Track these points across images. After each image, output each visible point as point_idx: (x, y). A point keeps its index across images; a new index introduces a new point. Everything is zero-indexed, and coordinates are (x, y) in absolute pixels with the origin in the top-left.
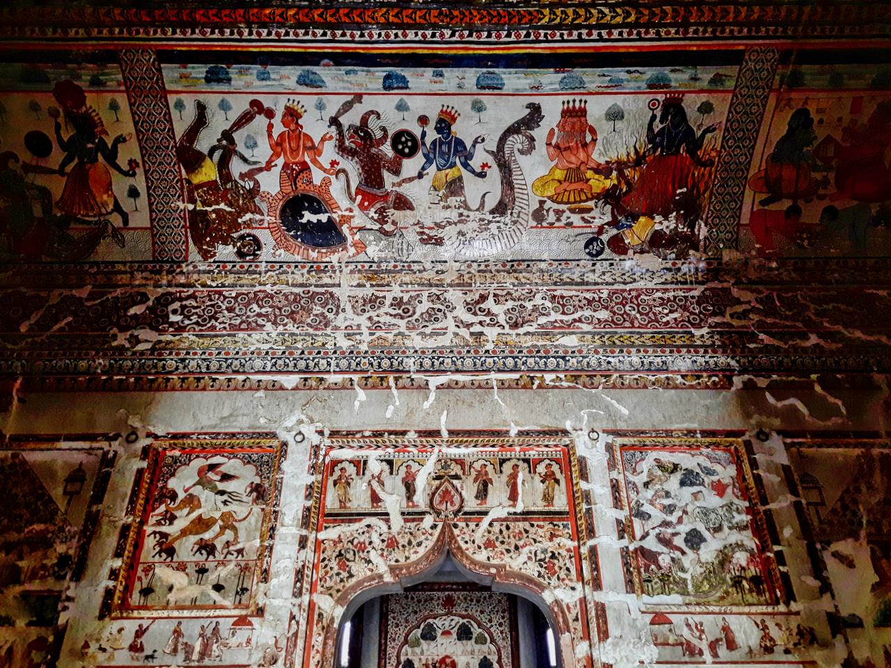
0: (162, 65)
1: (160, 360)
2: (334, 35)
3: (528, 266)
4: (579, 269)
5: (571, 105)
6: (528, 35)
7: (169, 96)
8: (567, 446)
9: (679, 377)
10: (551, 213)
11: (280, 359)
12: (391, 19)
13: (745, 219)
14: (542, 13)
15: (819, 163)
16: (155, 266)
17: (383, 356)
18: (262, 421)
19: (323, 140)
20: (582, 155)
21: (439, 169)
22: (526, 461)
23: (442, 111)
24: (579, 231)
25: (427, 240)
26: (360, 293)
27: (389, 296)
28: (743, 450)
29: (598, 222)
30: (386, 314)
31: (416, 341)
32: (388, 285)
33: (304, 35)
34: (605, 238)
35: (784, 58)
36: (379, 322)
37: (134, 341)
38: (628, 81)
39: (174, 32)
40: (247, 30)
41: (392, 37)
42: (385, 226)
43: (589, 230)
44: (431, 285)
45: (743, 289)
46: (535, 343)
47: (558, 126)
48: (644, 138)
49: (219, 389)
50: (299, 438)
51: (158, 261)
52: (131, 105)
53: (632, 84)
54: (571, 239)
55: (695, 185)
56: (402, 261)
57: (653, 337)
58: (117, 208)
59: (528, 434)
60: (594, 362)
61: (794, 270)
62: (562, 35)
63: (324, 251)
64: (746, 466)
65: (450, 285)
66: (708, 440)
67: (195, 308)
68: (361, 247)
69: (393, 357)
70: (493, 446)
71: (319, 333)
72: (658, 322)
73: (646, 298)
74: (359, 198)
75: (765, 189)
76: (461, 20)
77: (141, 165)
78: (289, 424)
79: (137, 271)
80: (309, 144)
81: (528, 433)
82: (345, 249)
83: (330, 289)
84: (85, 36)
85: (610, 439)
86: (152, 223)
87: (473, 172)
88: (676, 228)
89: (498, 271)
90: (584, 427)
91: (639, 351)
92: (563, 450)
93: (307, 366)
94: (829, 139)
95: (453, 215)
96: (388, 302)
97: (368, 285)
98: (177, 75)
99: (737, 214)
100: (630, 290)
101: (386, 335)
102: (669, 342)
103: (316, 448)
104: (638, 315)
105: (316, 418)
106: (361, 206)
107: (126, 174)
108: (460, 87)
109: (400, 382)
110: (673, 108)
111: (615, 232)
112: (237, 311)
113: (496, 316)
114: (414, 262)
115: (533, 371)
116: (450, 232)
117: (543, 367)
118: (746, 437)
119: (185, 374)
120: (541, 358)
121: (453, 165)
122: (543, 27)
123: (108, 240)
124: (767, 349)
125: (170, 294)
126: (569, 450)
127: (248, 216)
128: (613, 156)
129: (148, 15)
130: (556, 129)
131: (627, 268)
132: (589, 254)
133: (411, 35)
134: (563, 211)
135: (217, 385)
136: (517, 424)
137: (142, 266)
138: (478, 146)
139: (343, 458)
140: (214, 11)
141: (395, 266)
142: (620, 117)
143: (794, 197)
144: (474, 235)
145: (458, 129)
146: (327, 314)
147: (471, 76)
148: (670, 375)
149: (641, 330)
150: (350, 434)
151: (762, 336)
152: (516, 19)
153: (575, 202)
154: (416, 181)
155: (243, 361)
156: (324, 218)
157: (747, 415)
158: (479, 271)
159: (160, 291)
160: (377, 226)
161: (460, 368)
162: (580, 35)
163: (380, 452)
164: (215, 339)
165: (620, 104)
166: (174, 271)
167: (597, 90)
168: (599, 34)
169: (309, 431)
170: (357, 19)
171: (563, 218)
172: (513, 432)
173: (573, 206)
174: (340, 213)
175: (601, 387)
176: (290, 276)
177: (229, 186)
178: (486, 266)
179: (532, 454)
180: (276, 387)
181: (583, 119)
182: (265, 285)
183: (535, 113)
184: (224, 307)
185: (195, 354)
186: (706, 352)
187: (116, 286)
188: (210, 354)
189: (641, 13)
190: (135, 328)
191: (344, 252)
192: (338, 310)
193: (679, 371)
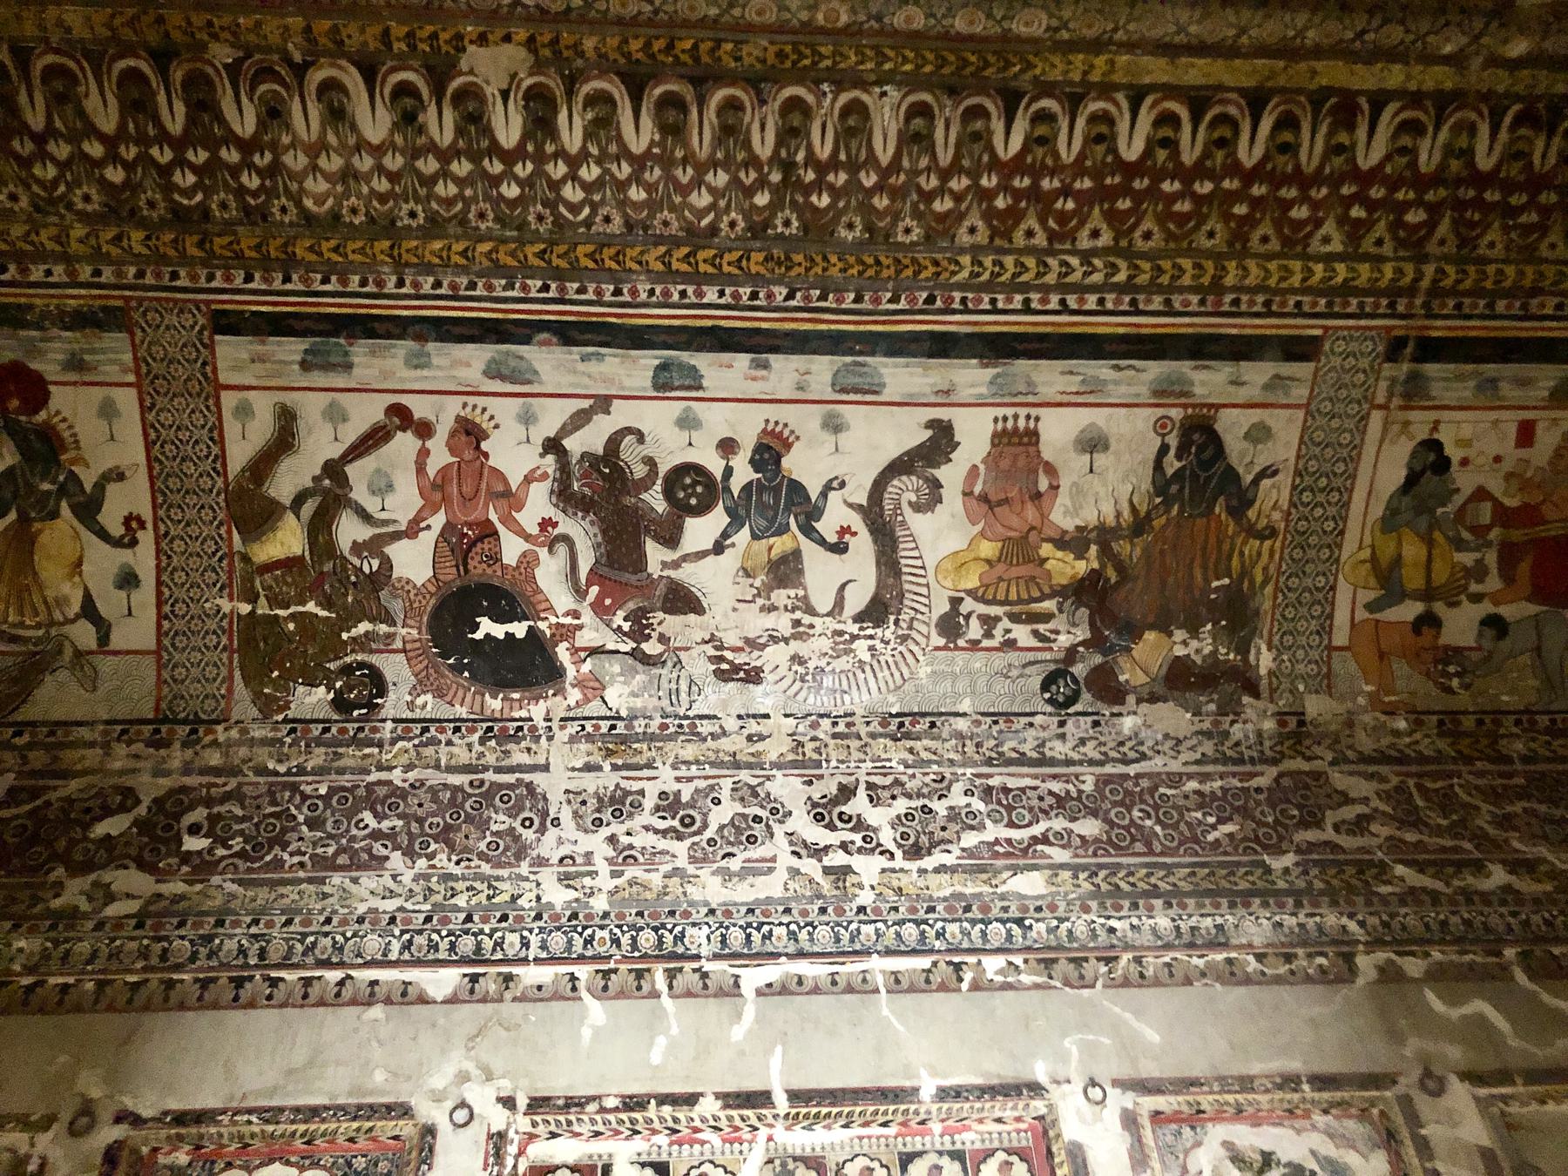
0: (218, 338)
1: (159, 939)
2: (562, 289)
3: (933, 725)
4: (1032, 732)
5: (1010, 424)
6: (930, 300)
7: (224, 394)
8: (1041, 1118)
9: (1251, 958)
10: (974, 623)
11: (420, 932)
12: (675, 265)
13: (1340, 638)
14: (957, 263)
15: (1466, 535)
16: (157, 731)
17: (640, 922)
18: (379, 1077)
19: (528, 480)
20: (1031, 513)
21: (755, 537)
22: (957, 1156)
23: (764, 431)
24: (1030, 656)
25: (727, 673)
26: (590, 783)
27: (652, 790)
28: (1399, 1119)
29: (1064, 640)
30: (646, 828)
31: (710, 888)
32: (649, 765)
33: (505, 289)
34: (1079, 670)
35: (1395, 349)
36: (631, 847)
37: (100, 894)
38: (1116, 383)
39: (249, 278)
40: (394, 278)
41: (676, 297)
42: (644, 646)
43: (1048, 656)
44: (737, 765)
45: (1351, 774)
46: (959, 888)
47: (984, 461)
48: (1146, 485)
49: (282, 1005)
50: (461, 1116)
51: (165, 720)
52: (144, 410)
53: (1123, 389)
54: (1014, 673)
55: (1245, 572)
56: (676, 716)
57: (1193, 874)
58: (89, 610)
59: (958, 1095)
60: (1081, 929)
61: (1441, 735)
62: (993, 301)
63: (516, 696)
64: (1409, 1152)
65: (777, 765)
66: (1326, 1095)
67: (243, 819)
68: (594, 687)
69: (663, 926)
70: (885, 1124)
71: (504, 873)
72: (1197, 842)
73: (1169, 792)
74: (595, 590)
75: (1372, 582)
76: (807, 270)
77: (150, 526)
78: (438, 1082)
79: (118, 740)
80: (500, 488)
81: (957, 1093)
82: (561, 692)
83: (527, 777)
84: (66, 279)
85: (1129, 1100)
86: (159, 641)
87: (822, 542)
88: (1215, 652)
89: (873, 736)
90: (1074, 1076)
91: (1169, 905)
92: (1032, 1128)
93: (479, 947)
94: (1481, 494)
95: (782, 623)
96: (649, 803)
97: (607, 767)
98: (245, 356)
99: (1326, 627)
100: (1138, 776)
101: (647, 876)
102: (1224, 884)
103: (498, 1140)
104: (1158, 829)
105: (497, 1065)
106: (598, 607)
107: (117, 543)
108: (800, 388)
109: (679, 982)
110: (1199, 433)
111: (1098, 659)
112: (329, 826)
113: (875, 830)
114: (701, 717)
115: (957, 951)
116: (775, 656)
117: (979, 943)
118: (1400, 1089)
119: (212, 969)
120: (973, 922)
121: (783, 530)
122: (961, 287)
123: (62, 675)
124: (1412, 895)
125: (184, 789)
126: (1045, 1128)
127: (364, 627)
128: (1089, 517)
129: (200, 245)
130: (982, 467)
131: (1126, 731)
132: (1050, 701)
133: (711, 295)
134: (997, 619)
135: (280, 994)
136: (934, 1073)
137: (125, 728)
138: (832, 495)
139: (557, 1161)
140: (333, 243)
141: (664, 727)
142: (1101, 444)
143: (1428, 595)
144: (823, 663)
145: (796, 464)
146: (520, 830)
147: (822, 368)
148: (1233, 955)
149: (1168, 860)
150: (574, 1103)
151: (1400, 870)
152: (909, 272)
153: (1020, 601)
154: (711, 560)
155: (339, 938)
156: (519, 629)
157: (1395, 1037)
158: (835, 736)
159: (165, 783)
160: (628, 646)
161: (807, 947)
162: (1027, 301)
163: (639, 1145)
164: (282, 890)
165: (1101, 423)
166: (199, 740)
167: (1059, 398)
168: (1063, 302)
169: (482, 1098)
170: (610, 264)
171: (998, 632)
172: (927, 1092)
173: (1016, 609)
174: (553, 620)
175: (1099, 984)
176: (443, 749)
177: (328, 567)
178: (848, 725)
179: (969, 1140)
180: (408, 996)
181: (1032, 449)
182: (390, 769)
183: (941, 442)
184: (301, 818)
185: (236, 924)
186: (1299, 904)
187: (66, 775)
188: (270, 924)
189: (1137, 267)
190: (103, 867)
191: (559, 698)
192: (546, 821)
193: (1250, 946)
